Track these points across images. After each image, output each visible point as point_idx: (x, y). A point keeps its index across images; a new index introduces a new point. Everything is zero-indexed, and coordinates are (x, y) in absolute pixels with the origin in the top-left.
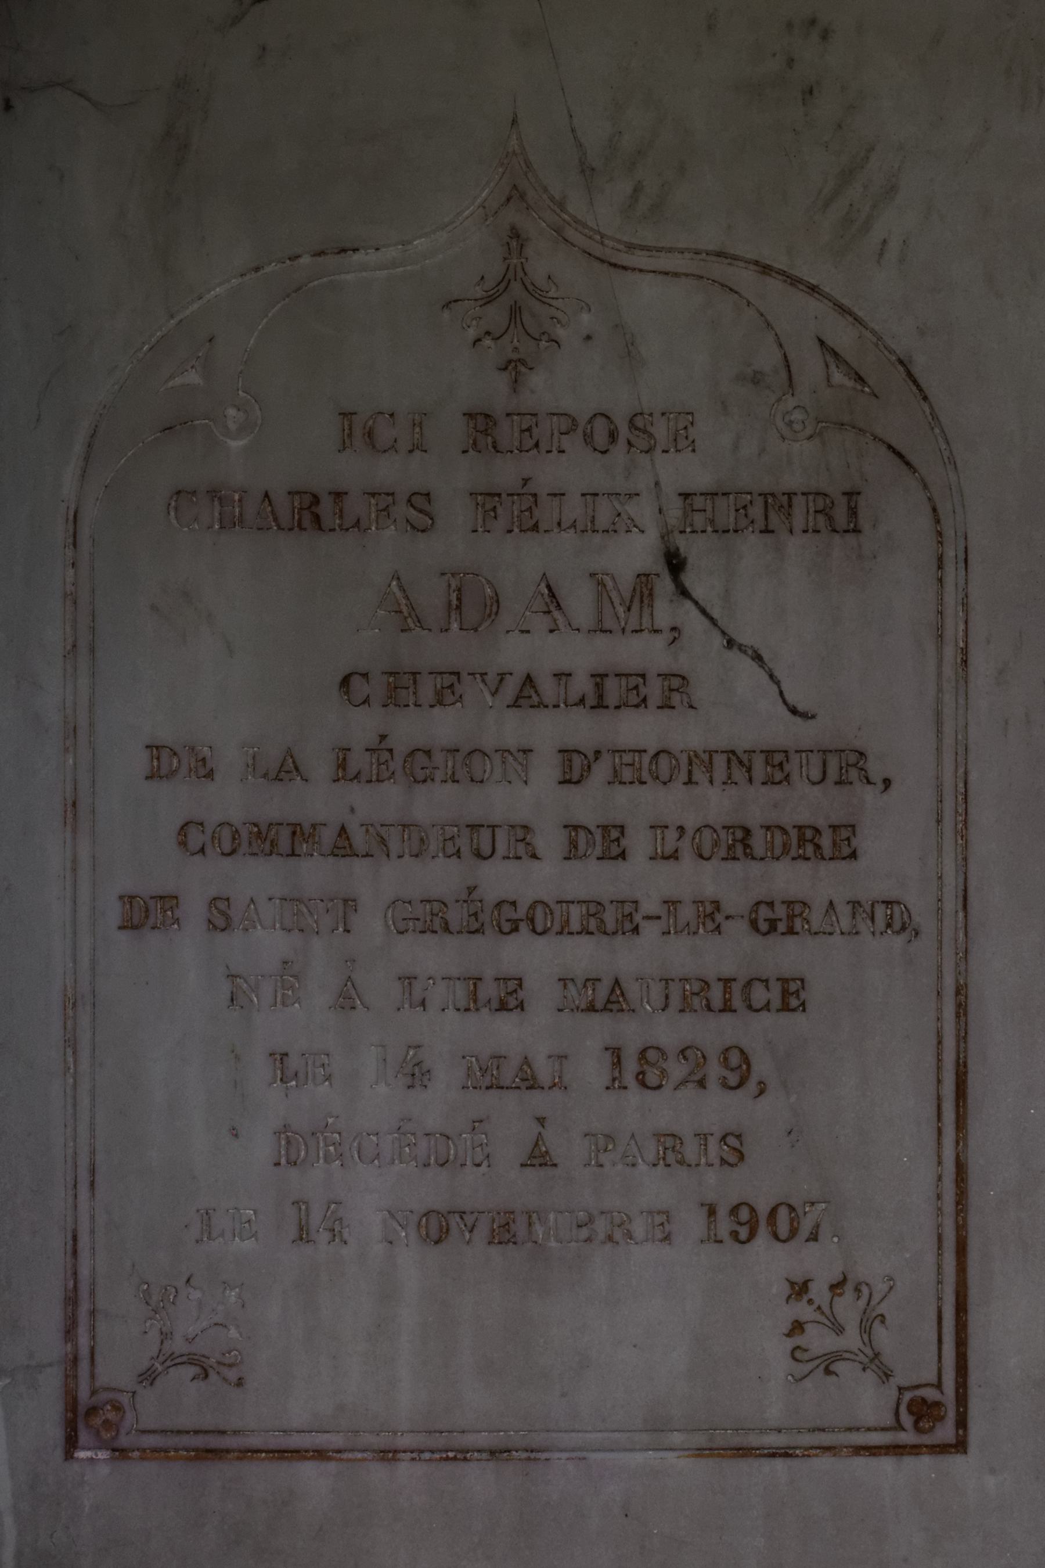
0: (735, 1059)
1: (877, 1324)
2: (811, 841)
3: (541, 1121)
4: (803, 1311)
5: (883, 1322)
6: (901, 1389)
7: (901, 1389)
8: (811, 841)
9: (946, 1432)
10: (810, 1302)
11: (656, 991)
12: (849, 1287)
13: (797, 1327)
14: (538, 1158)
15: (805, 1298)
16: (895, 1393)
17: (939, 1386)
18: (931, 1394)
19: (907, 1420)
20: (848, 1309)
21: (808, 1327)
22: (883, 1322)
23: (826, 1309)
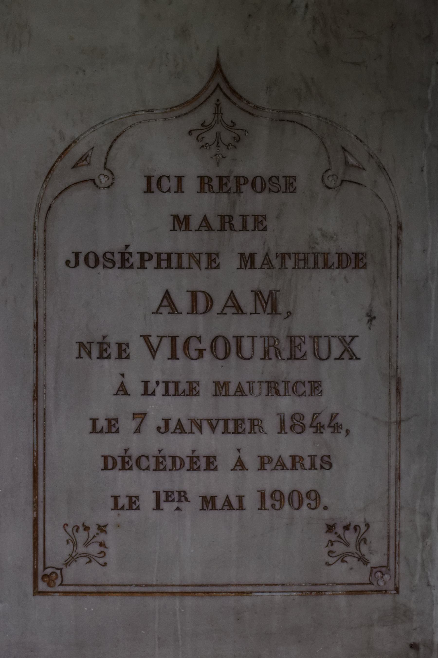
0: (277, 496)
1: (363, 542)
2: (183, 496)
3: (123, 375)
4: (93, 530)
5: (365, 543)
6: (61, 570)
7: (61, 570)
8: (183, 496)
9: (42, 586)
10: (336, 533)
11: (162, 386)
12: (102, 549)
13: (86, 528)
14: (123, 390)
15: (99, 532)
16: (60, 567)
17: (61, 585)
18: (58, 581)
19: (49, 571)
20: (94, 549)
21: (86, 532)
22: (365, 543)
23: (94, 540)
